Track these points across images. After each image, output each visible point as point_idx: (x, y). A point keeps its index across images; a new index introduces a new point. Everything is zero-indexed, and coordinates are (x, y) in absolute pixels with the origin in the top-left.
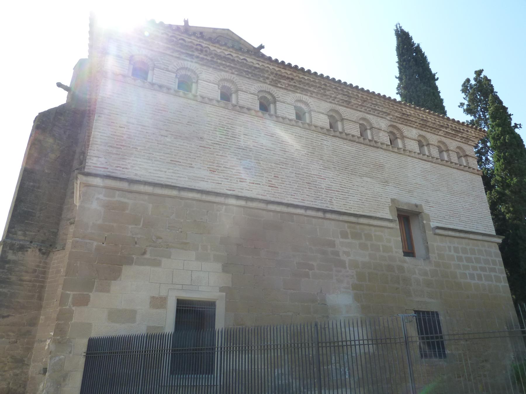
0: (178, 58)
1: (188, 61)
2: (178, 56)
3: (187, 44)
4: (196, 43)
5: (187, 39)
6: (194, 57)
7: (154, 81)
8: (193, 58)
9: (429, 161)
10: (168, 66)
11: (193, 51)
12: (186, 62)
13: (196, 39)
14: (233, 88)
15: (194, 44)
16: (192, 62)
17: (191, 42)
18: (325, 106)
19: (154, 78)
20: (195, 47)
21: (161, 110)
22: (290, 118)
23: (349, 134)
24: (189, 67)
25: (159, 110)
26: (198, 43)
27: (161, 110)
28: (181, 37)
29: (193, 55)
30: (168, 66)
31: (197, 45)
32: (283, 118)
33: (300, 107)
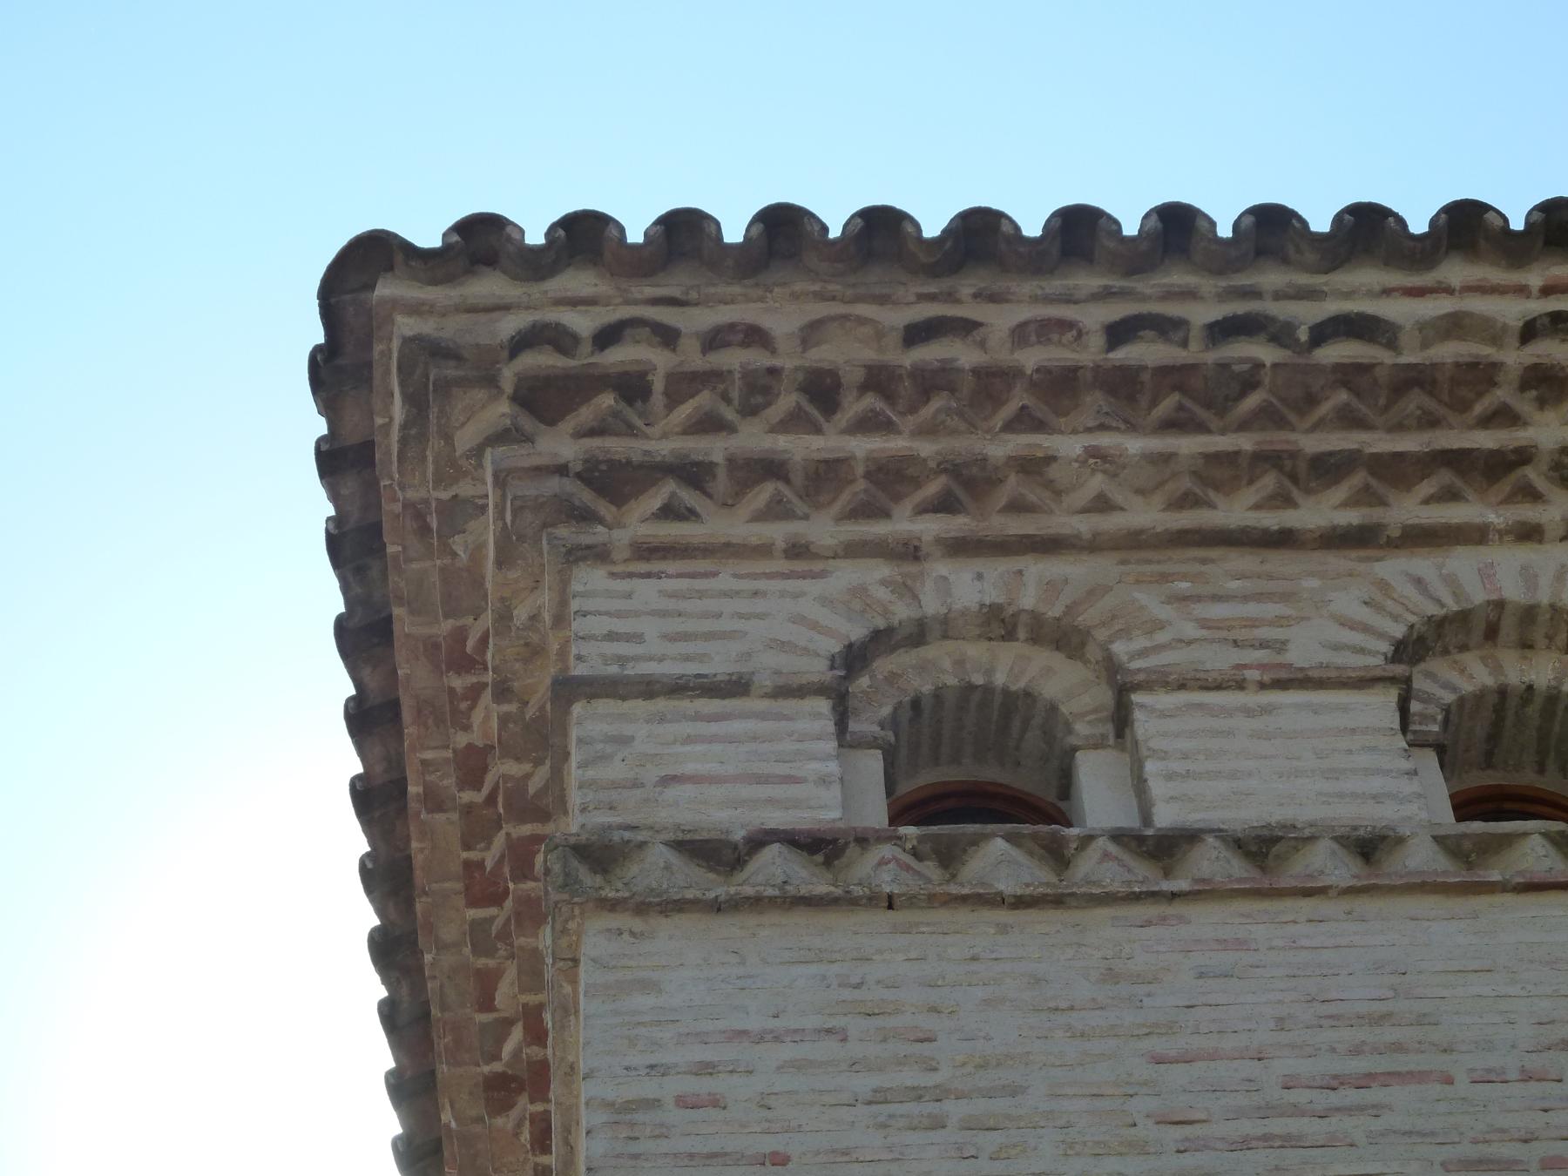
0: (1360, 539)
1: (1477, 535)
2: (1352, 517)
3: (1410, 356)
4: (1512, 311)
5: (1396, 310)
6: (1533, 474)
7: (1166, 817)
8: (1532, 494)
9: (1135, 898)
10: (1281, 646)
11: (1504, 416)
12: (1463, 562)
13: (1117, 283)
14: (1065, 684)
15: (1491, 331)
16: (1529, 534)
17: (1454, 326)
18: (795, 615)
19: (1157, 788)
20: (1515, 358)
21: (1365, 1081)
22: (822, 809)
23: (1186, 838)
24: (1513, 592)
25: (1334, 1084)
26: (1538, 307)
27: (1365, 1081)
28: (1332, 307)
29: (1523, 456)
30: (1281, 646)
31: (1529, 332)
32: (1261, 847)
33: (1502, 703)
